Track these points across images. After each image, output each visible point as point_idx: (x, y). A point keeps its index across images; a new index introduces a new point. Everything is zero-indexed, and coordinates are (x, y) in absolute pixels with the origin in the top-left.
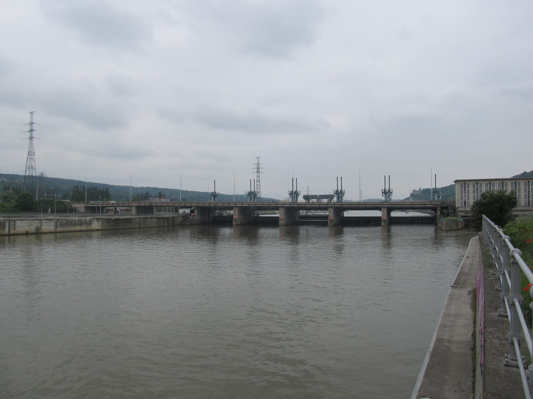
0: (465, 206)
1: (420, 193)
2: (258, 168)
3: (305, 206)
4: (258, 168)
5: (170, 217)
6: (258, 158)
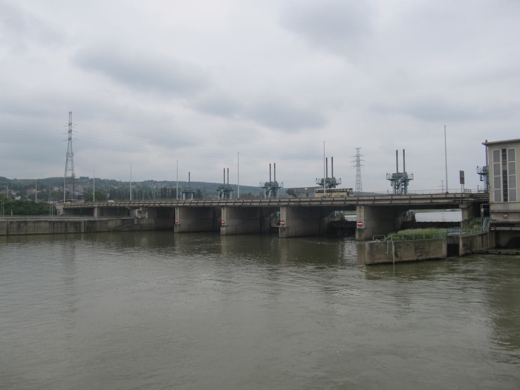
0: (506, 200)
2: (358, 161)
3: (211, 205)
4: (358, 161)
5: (82, 221)
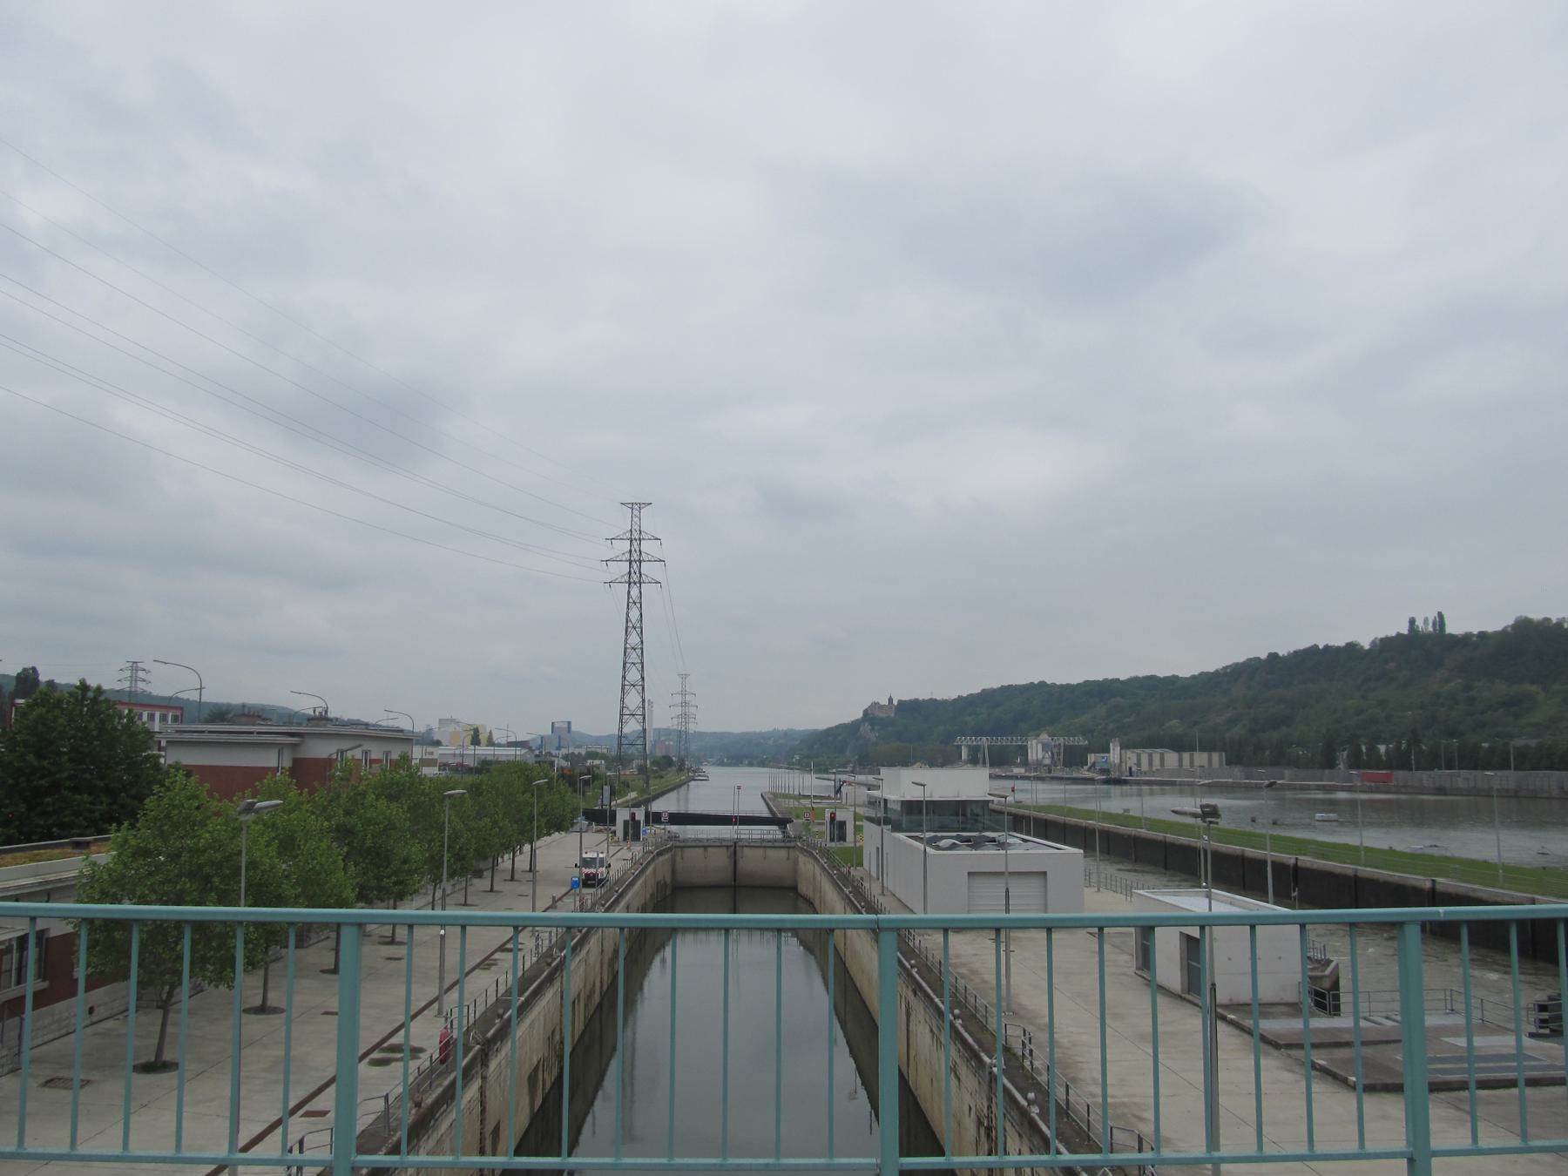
1: (892, 715)
2: (635, 560)
4: (635, 560)
6: (636, 507)
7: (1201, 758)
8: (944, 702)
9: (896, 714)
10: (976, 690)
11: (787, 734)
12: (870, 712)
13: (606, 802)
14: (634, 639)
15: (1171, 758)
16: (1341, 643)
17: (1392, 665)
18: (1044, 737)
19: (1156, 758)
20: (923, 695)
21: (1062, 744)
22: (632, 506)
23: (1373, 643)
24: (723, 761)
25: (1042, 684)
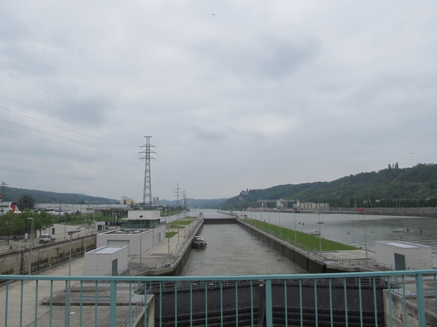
1: (248, 194)
2: (148, 153)
4: (148, 153)
7: (322, 205)
8: (263, 190)
9: (249, 194)
10: (271, 187)
11: (222, 200)
12: (242, 193)
13: (116, 219)
14: (148, 174)
15: (314, 205)
16: (370, 172)
17: (383, 178)
18: (281, 199)
19: (310, 205)
20: (257, 188)
21: (287, 201)
22: (147, 137)
23: (379, 171)
24: (203, 207)
25: (290, 184)
